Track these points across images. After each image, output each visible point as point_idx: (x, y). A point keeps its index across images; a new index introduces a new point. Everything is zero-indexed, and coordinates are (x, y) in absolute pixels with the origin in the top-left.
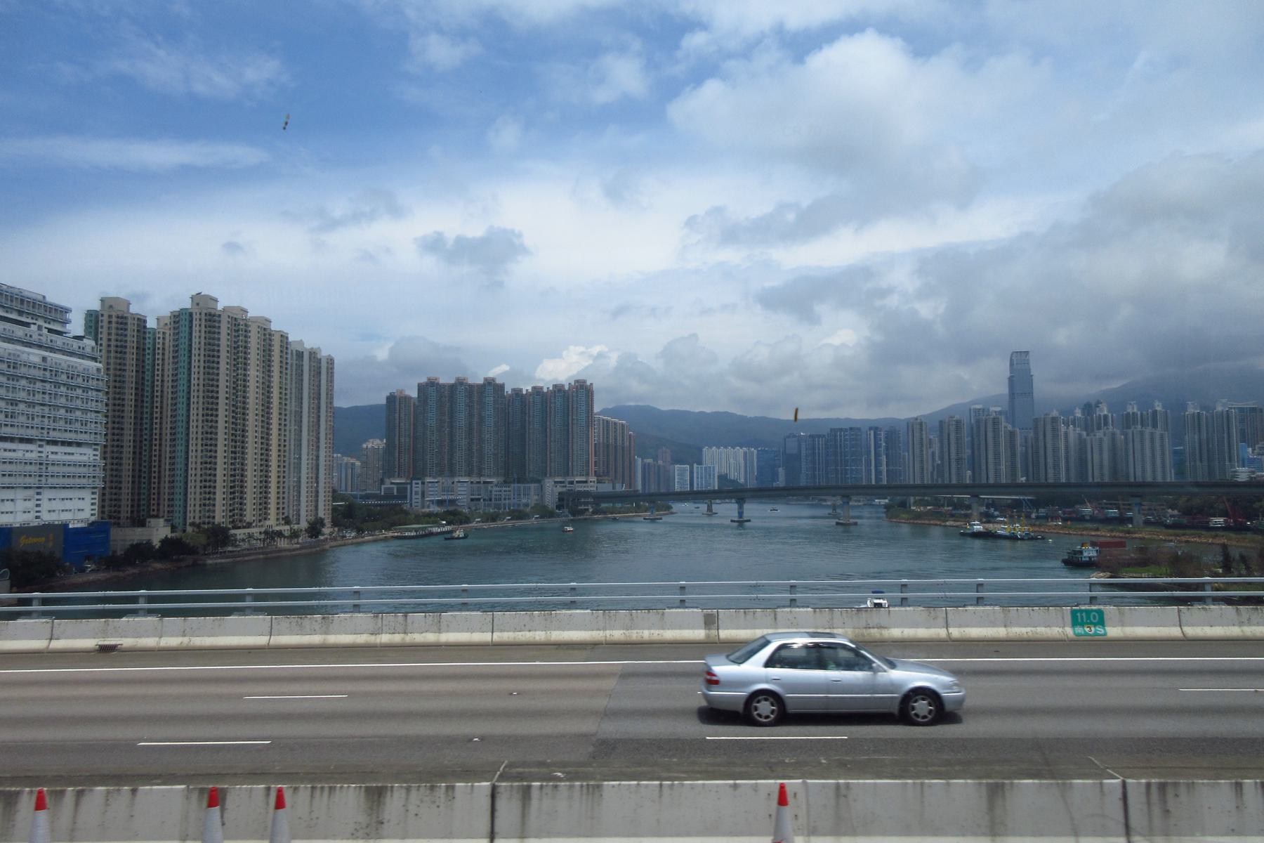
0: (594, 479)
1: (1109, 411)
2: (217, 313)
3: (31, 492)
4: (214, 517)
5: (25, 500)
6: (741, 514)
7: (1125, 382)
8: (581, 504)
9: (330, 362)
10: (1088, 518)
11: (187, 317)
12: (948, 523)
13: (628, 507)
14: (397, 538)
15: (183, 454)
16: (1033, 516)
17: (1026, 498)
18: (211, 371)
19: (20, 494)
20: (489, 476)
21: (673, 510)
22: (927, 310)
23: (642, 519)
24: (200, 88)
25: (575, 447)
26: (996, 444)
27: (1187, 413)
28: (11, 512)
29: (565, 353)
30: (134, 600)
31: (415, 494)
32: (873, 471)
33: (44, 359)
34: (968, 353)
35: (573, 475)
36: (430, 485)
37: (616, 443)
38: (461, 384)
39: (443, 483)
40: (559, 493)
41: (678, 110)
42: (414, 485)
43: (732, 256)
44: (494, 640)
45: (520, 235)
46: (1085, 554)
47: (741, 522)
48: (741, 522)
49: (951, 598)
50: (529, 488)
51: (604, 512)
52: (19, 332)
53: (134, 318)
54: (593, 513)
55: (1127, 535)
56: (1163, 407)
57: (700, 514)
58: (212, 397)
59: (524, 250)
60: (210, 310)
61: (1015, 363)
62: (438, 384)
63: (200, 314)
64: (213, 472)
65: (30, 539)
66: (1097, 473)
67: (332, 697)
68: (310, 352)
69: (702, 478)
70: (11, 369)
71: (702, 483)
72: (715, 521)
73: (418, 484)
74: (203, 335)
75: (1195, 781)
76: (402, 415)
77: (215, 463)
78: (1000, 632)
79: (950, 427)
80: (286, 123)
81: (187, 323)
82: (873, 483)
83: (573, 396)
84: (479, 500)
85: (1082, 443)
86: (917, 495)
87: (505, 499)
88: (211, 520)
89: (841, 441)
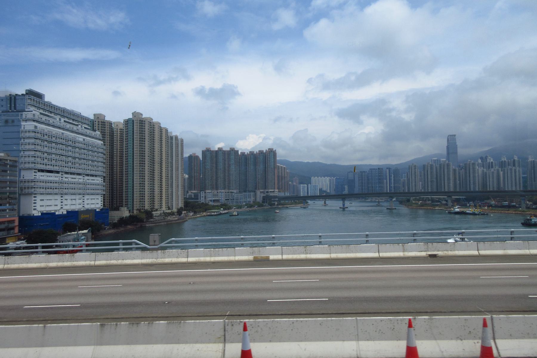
0: (277, 190)
1: (493, 160)
2: (144, 120)
3: (81, 196)
4: (145, 207)
5: (79, 199)
6: (344, 205)
7: (491, 148)
8: (272, 201)
9: (182, 141)
10: (494, 206)
12: (436, 208)
14: (209, 215)
15: (131, 180)
17: (463, 197)
18: (142, 145)
19: (78, 197)
21: (309, 204)
22: (408, 117)
24: (91, 26)
26: (448, 175)
27: (528, 161)
28: (75, 205)
29: (247, 138)
30: (118, 244)
31: (203, 196)
33: (84, 140)
35: (268, 189)
36: (208, 193)
37: (282, 175)
38: (271, 151)
39: (213, 192)
40: (263, 197)
41: (308, 33)
42: (201, 194)
43: (326, 95)
45: (236, 87)
46: (533, 220)
47: (344, 209)
48: (344, 209)
49: (500, 237)
50: (250, 194)
51: (282, 205)
52: (75, 128)
53: (108, 123)
54: (277, 205)
55: (523, 213)
56: (518, 158)
58: (142, 156)
59: (238, 94)
60: (141, 119)
61: (450, 139)
62: (235, 151)
63: (137, 120)
64: (143, 188)
69: (312, 190)
70: (73, 144)
71: (312, 193)
72: (327, 208)
73: (203, 193)
74: (138, 129)
76: (195, 164)
77: (145, 184)
79: (428, 167)
82: (388, 191)
83: (268, 155)
84: (229, 199)
85: (484, 175)
86: (413, 197)
87: (240, 199)
88: (144, 208)
89: (374, 174)
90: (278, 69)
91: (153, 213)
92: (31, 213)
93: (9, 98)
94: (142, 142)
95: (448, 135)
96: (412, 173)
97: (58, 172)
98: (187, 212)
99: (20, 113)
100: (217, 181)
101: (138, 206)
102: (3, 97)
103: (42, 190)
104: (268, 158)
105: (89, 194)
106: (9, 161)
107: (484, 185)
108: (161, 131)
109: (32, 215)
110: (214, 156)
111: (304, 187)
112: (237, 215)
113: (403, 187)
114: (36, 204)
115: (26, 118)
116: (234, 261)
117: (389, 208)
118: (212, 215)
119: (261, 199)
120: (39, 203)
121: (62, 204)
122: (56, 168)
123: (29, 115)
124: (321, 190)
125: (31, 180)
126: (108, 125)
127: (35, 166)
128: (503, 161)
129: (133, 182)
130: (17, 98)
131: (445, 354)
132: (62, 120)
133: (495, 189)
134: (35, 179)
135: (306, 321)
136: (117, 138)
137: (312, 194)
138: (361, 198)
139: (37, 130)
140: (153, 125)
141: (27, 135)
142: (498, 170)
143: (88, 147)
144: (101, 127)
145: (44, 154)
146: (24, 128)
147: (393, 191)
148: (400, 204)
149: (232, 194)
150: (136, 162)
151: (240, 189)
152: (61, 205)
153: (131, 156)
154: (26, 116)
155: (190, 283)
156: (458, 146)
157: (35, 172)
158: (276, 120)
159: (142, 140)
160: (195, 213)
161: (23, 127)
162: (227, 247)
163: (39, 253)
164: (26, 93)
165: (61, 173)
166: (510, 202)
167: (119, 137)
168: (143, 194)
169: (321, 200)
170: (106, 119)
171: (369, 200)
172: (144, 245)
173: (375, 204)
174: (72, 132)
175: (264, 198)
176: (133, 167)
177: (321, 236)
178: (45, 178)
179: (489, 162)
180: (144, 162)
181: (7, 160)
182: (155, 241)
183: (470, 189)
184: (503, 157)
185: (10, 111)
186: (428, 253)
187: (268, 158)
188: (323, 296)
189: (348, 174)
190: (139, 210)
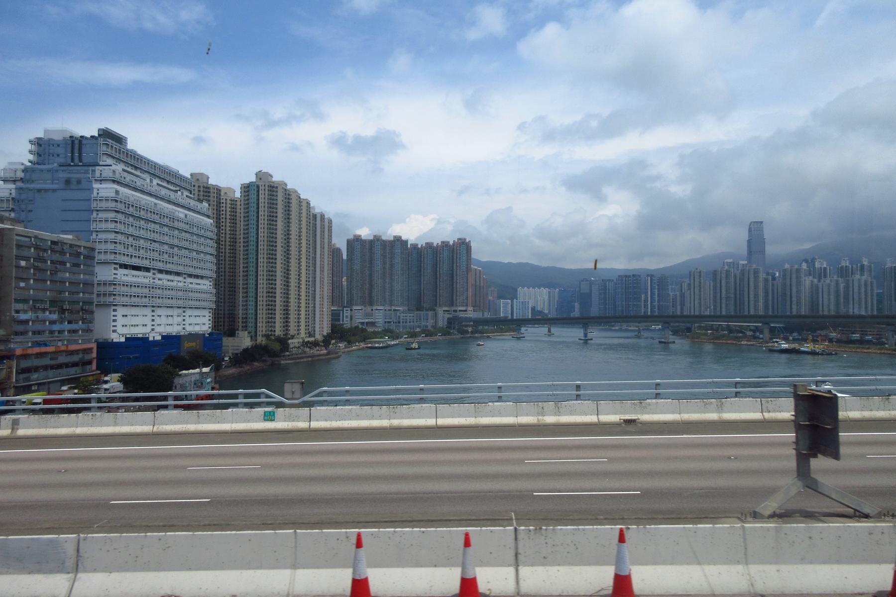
1: (850, 264)
2: (275, 186)
3: (180, 311)
4: (275, 331)
9: (330, 222)
11: (255, 188)
12: (743, 343)
13: (492, 329)
14: (370, 348)
16: (791, 338)
19: (176, 312)
20: (397, 306)
22: (680, 191)
23: (511, 337)
24: (148, 25)
25: (458, 286)
26: (756, 287)
29: (407, 220)
30: (236, 396)
32: (649, 305)
33: (186, 216)
34: (708, 223)
35: (456, 306)
36: (356, 311)
38: (378, 240)
41: (524, 48)
42: (345, 312)
43: (547, 150)
44: (438, 423)
47: (586, 341)
48: (586, 341)
50: (427, 315)
51: (481, 332)
53: (214, 189)
56: (869, 263)
57: (543, 335)
58: (272, 246)
59: (403, 146)
61: (753, 229)
62: (361, 240)
63: (265, 186)
65: (189, 343)
66: (826, 309)
67: (249, 468)
68: (321, 215)
69: (520, 309)
71: (520, 314)
73: (348, 310)
75: (630, 527)
77: (275, 293)
78: (385, 423)
80: (209, 49)
81: (255, 192)
82: (649, 314)
85: (815, 290)
90: (471, 105)
91: (290, 341)
92: (108, 337)
93: (70, 142)
94: (272, 223)
95: (750, 221)
96: (696, 283)
97: (147, 270)
98: (336, 342)
99: (91, 168)
100: (371, 290)
101: (264, 329)
102: (59, 141)
103: (125, 300)
104: (457, 255)
105: (192, 308)
106: (82, 248)
107: (814, 304)
108: (300, 206)
109: (110, 341)
110: (366, 249)
111: (506, 304)
112: (416, 349)
113: (673, 307)
114: (116, 321)
115: (101, 177)
116: (515, 424)
117: (663, 340)
118: (376, 348)
119: (446, 323)
120: (121, 321)
121: (153, 323)
122: (145, 263)
123: (107, 172)
124: (533, 309)
125: (109, 281)
126: (214, 193)
127: (115, 259)
128: (843, 266)
129: (257, 289)
130: (84, 142)
131: (718, 591)
132: (154, 182)
133: (833, 313)
134: (115, 280)
135: (491, 532)
136: (226, 215)
137: (519, 316)
138: (603, 324)
139: (119, 198)
140: (289, 195)
141: (104, 205)
142: (837, 281)
143: (191, 229)
144: (204, 196)
145: (128, 238)
146: (98, 193)
147: (657, 314)
148: (673, 335)
149: (396, 313)
150: (262, 256)
151: (408, 305)
152: (153, 325)
153: (253, 245)
154: (101, 174)
155: (60, 471)
156: (765, 240)
157: (115, 269)
158: (461, 192)
159: (272, 218)
160: (350, 343)
161: (95, 192)
162: (409, 402)
163: (169, 407)
164: (99, 135)
165: (152, 271)
166: (862, 334)
167: (228, 213)
168: (272, 310)
169: (536, 326)
170: (209, 183)
171: (617, 328)
172: (278, 398)
173: (633, 334)
174: (169, 202)
175: (450, 322)
176: (257, 264)
177: (423, 389)
178: (129, 279)
179: (821, 268)
180: (274, 257)
181: (80, 247)
182: (293, 393)
183: (791, 312)
184: (844, 260)
185: (72, 164)
186: (621, 418)
187: (457, 255)
188: (633, 488)
189: (580, 284)
190: (267, 337)
